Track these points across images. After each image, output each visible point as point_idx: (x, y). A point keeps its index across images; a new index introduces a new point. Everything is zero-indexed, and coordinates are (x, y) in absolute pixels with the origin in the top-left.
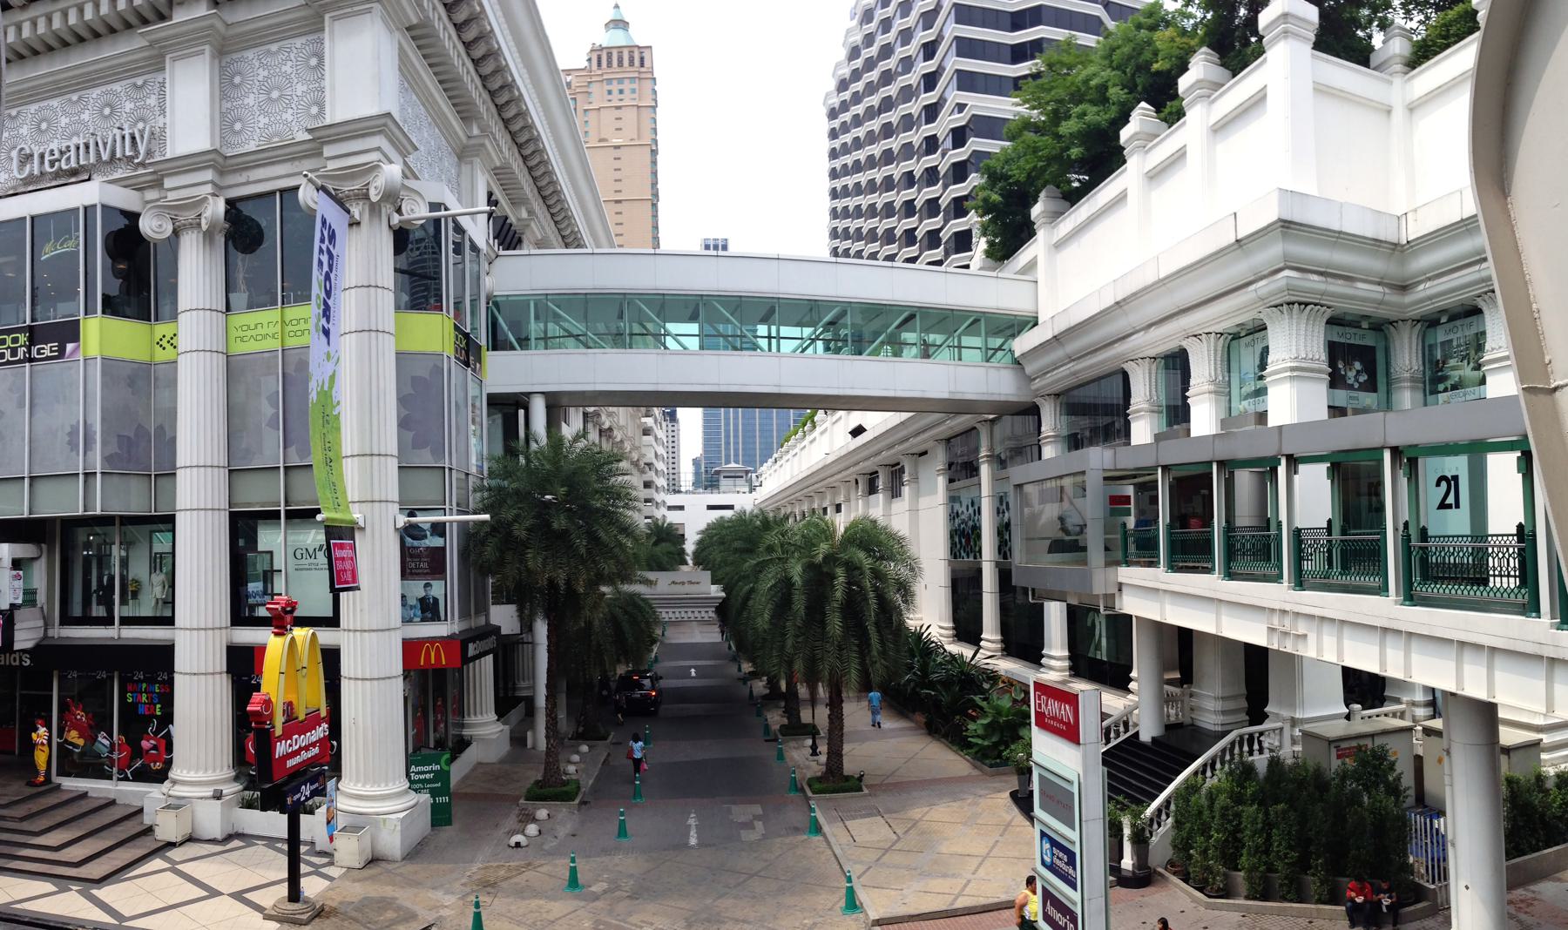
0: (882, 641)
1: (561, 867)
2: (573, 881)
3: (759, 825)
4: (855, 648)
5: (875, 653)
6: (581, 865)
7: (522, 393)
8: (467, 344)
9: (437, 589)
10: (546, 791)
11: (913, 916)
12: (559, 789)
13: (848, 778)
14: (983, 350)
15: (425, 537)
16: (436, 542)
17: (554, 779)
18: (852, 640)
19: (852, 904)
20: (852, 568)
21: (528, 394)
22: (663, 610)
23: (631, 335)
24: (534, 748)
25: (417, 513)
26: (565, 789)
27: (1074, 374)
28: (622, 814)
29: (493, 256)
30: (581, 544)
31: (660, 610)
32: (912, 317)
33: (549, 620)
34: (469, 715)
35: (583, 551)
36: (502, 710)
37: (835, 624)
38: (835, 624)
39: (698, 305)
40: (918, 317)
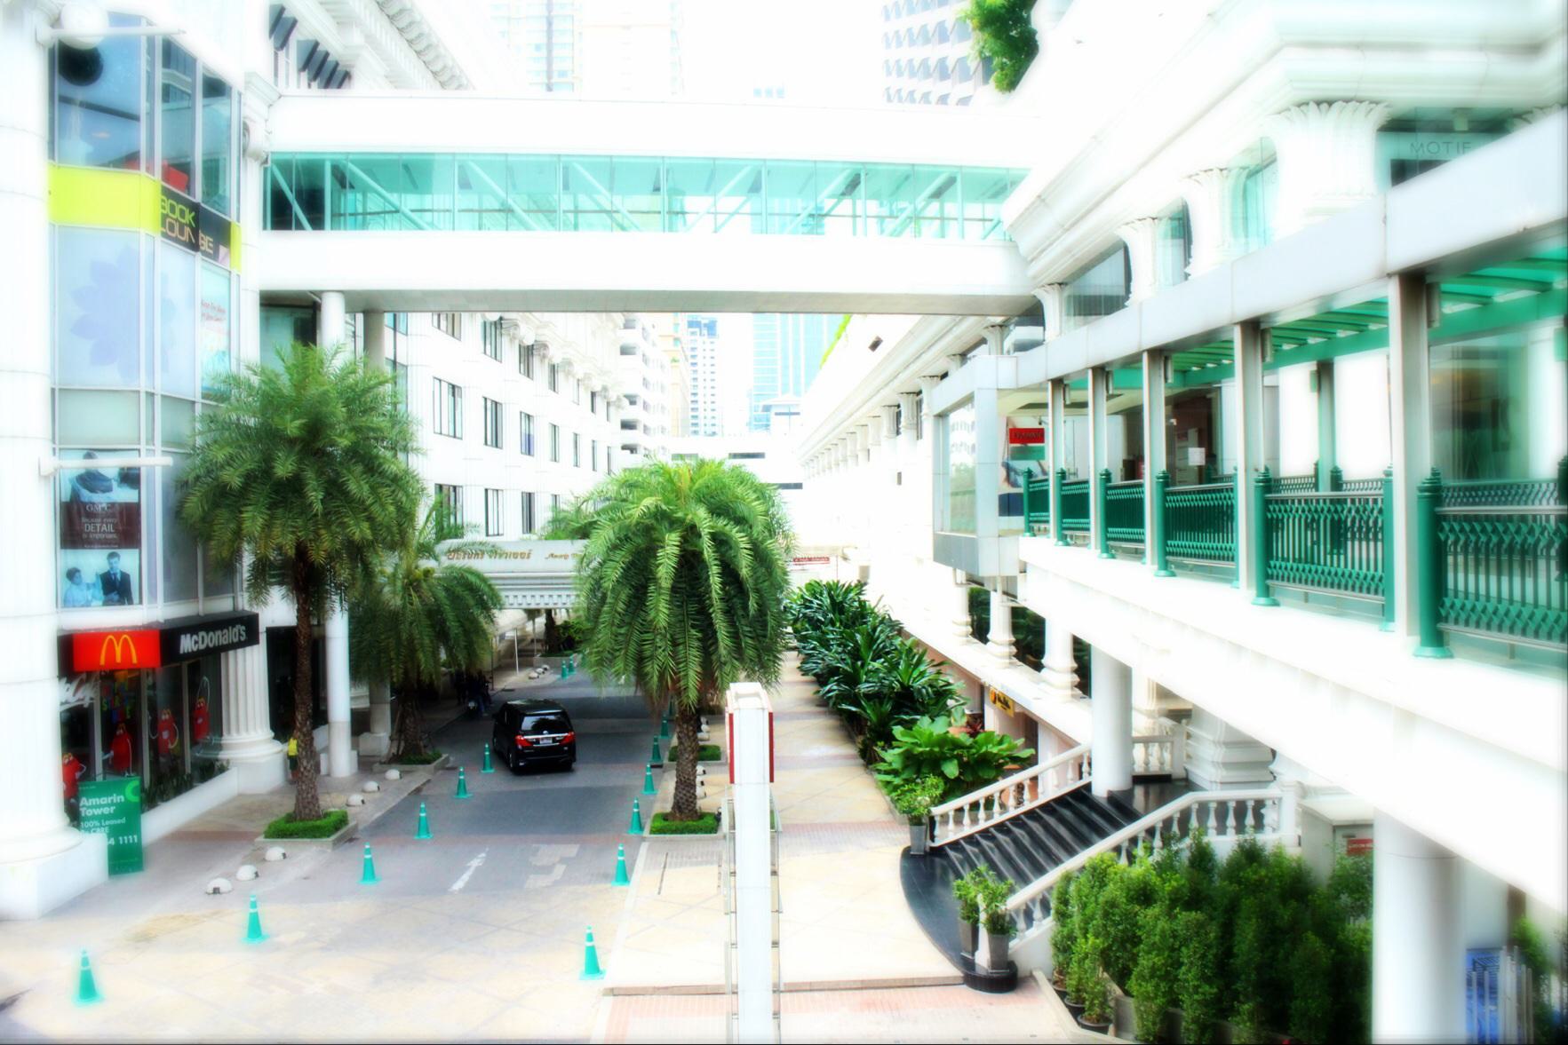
0: (735, 636)
1: (238, 916)
2: (255, 929)
3: (560, 869)
4: (696, 644)
5: (723, 651)
6: (264, 910)
7: (312, 292)
8: (196, 219)
9: (127, 561)
10: (292, 826)
11: (659, 989)
12: (310, 823)
13: (702, 816)
14: (960, 220)
15: (109, 489)
16: (123, 495)
17: (307, 811)
18: (693, 632)
19: (593, 967)
20: (690, 532)
21: (322, 292)
22: (511, 594)
23: (577, 211)
24: (328, 775)
25: (97, 454)
26: (318, 823)
27: (1068, 250)
28: (368, 851)
29: (275, 97)
30: (315, 496)
31: (507, 593)
32: (951, 181)
33: (298, 603)
34: (238, 730)
35: (318, 507)
36: (282, 725)
37: (661, 610)
38: (661, 610)
39: (759, 173)
40: (959, 180)
